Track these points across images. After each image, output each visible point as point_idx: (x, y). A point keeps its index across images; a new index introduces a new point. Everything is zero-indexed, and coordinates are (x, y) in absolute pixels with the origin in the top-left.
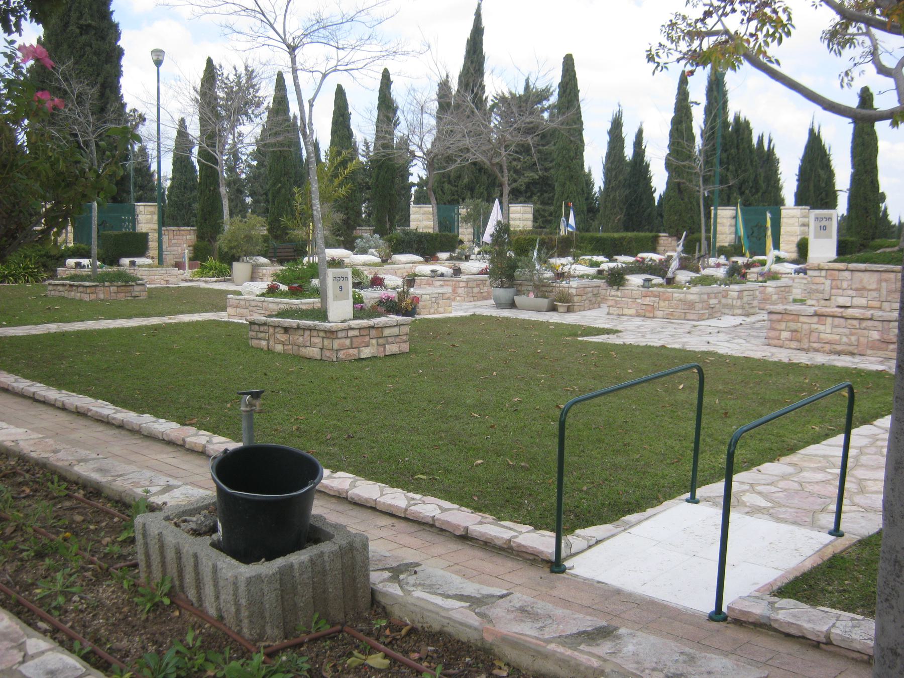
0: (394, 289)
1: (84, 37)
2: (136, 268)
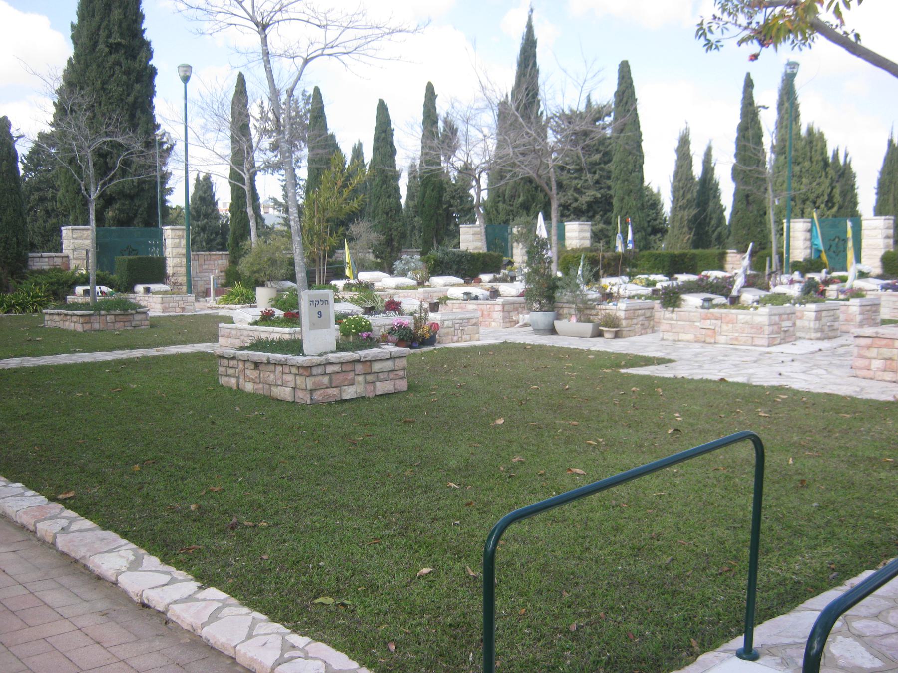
0: (411, 314)
1: (113, 56)
2: (150, 295)
